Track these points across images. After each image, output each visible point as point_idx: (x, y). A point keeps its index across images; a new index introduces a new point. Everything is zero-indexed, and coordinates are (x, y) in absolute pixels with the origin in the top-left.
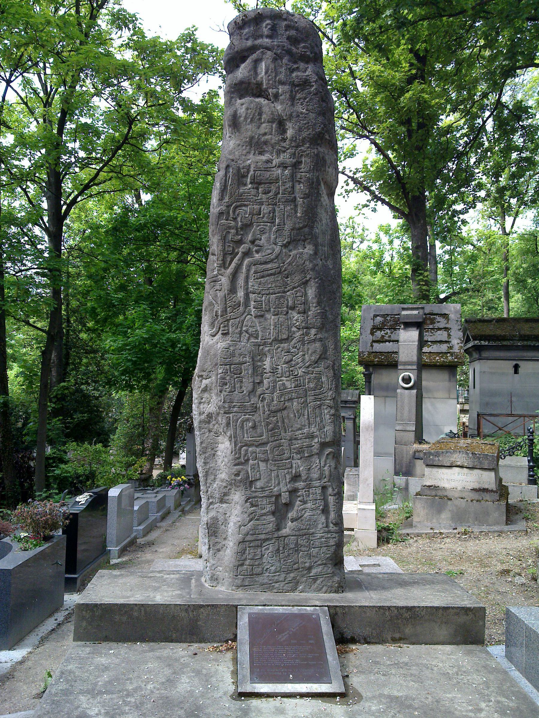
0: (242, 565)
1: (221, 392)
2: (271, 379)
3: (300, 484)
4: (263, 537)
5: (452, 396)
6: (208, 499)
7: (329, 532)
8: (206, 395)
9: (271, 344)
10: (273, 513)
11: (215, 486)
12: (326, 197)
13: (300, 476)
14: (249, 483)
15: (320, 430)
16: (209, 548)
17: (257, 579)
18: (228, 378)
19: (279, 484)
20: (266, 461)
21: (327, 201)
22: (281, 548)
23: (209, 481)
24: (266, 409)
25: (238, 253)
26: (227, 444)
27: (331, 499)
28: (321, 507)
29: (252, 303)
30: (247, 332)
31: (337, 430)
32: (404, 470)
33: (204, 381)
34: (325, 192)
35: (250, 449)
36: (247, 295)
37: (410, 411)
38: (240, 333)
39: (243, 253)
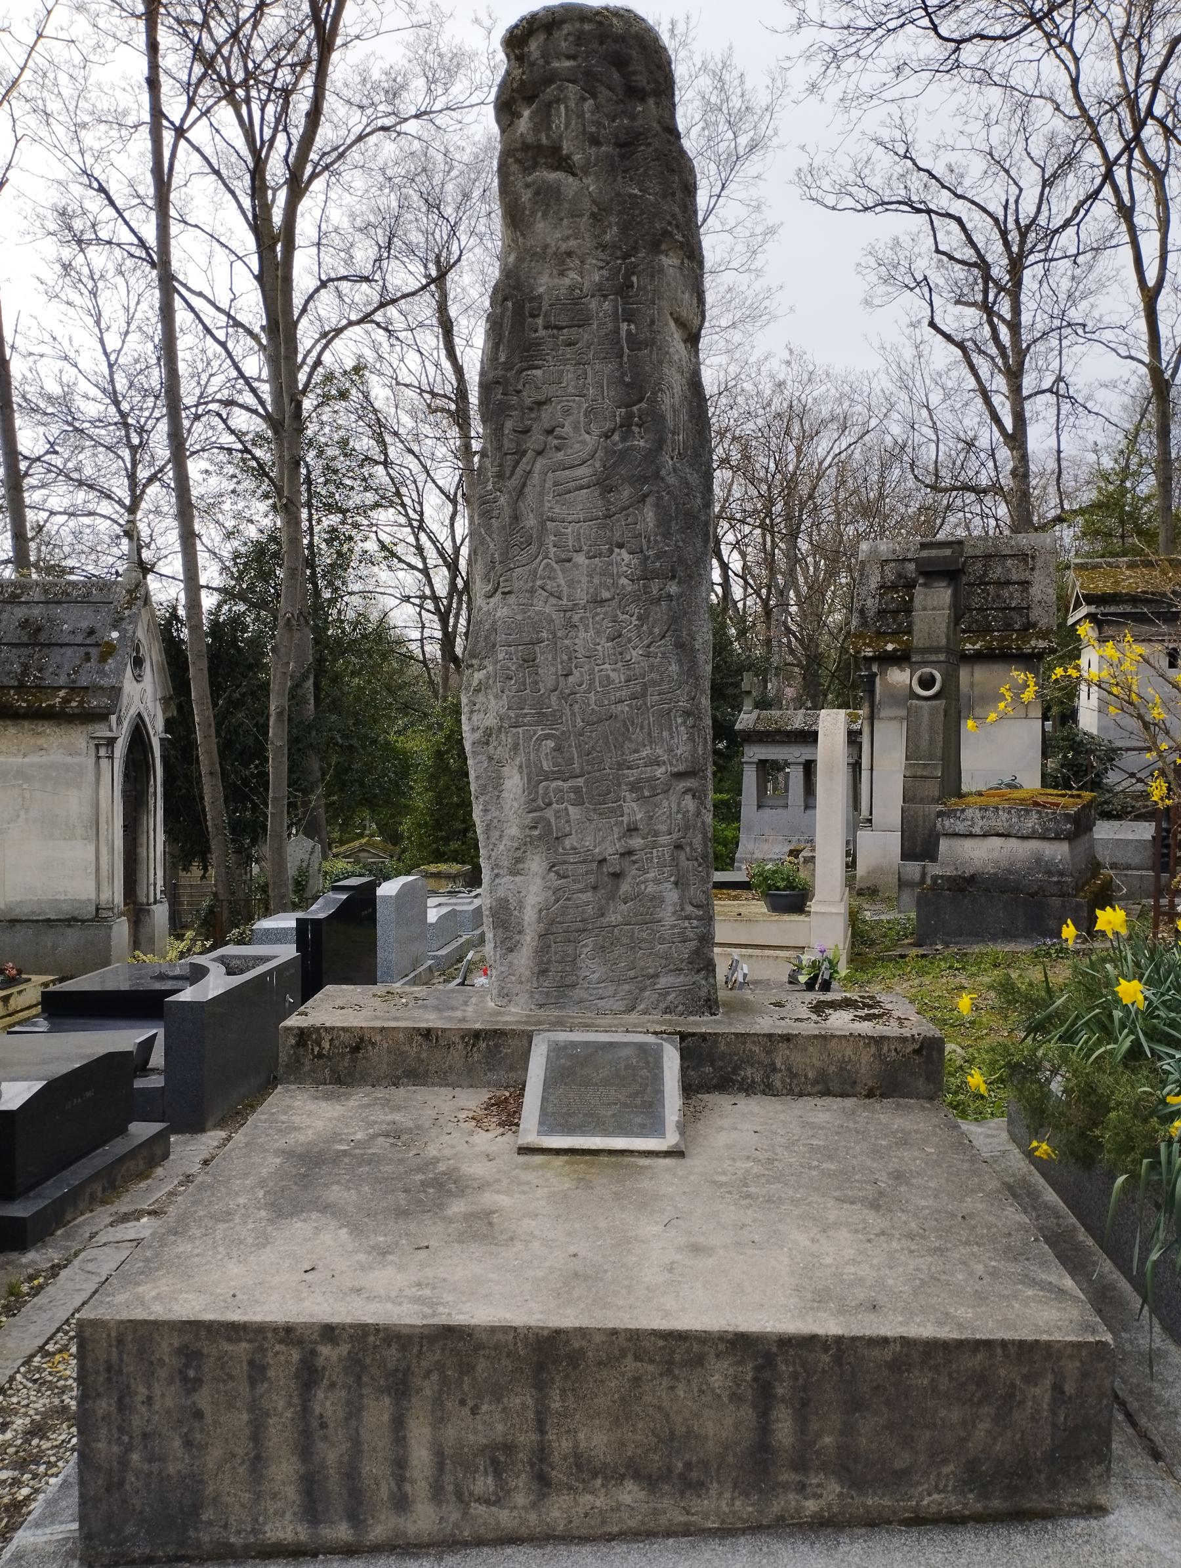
3: (636, 842)
7: (688, 918)
8: (481, 698)
9: (584, 608)
10: (595, 888)
11: (502, 847)
12: (681, 346)
13: (636, 829)
21: (684, 352)
25: (525, 452)
26: (517, 777)
33: (476, 675)
37: (932, 741)
38: (532, 591)
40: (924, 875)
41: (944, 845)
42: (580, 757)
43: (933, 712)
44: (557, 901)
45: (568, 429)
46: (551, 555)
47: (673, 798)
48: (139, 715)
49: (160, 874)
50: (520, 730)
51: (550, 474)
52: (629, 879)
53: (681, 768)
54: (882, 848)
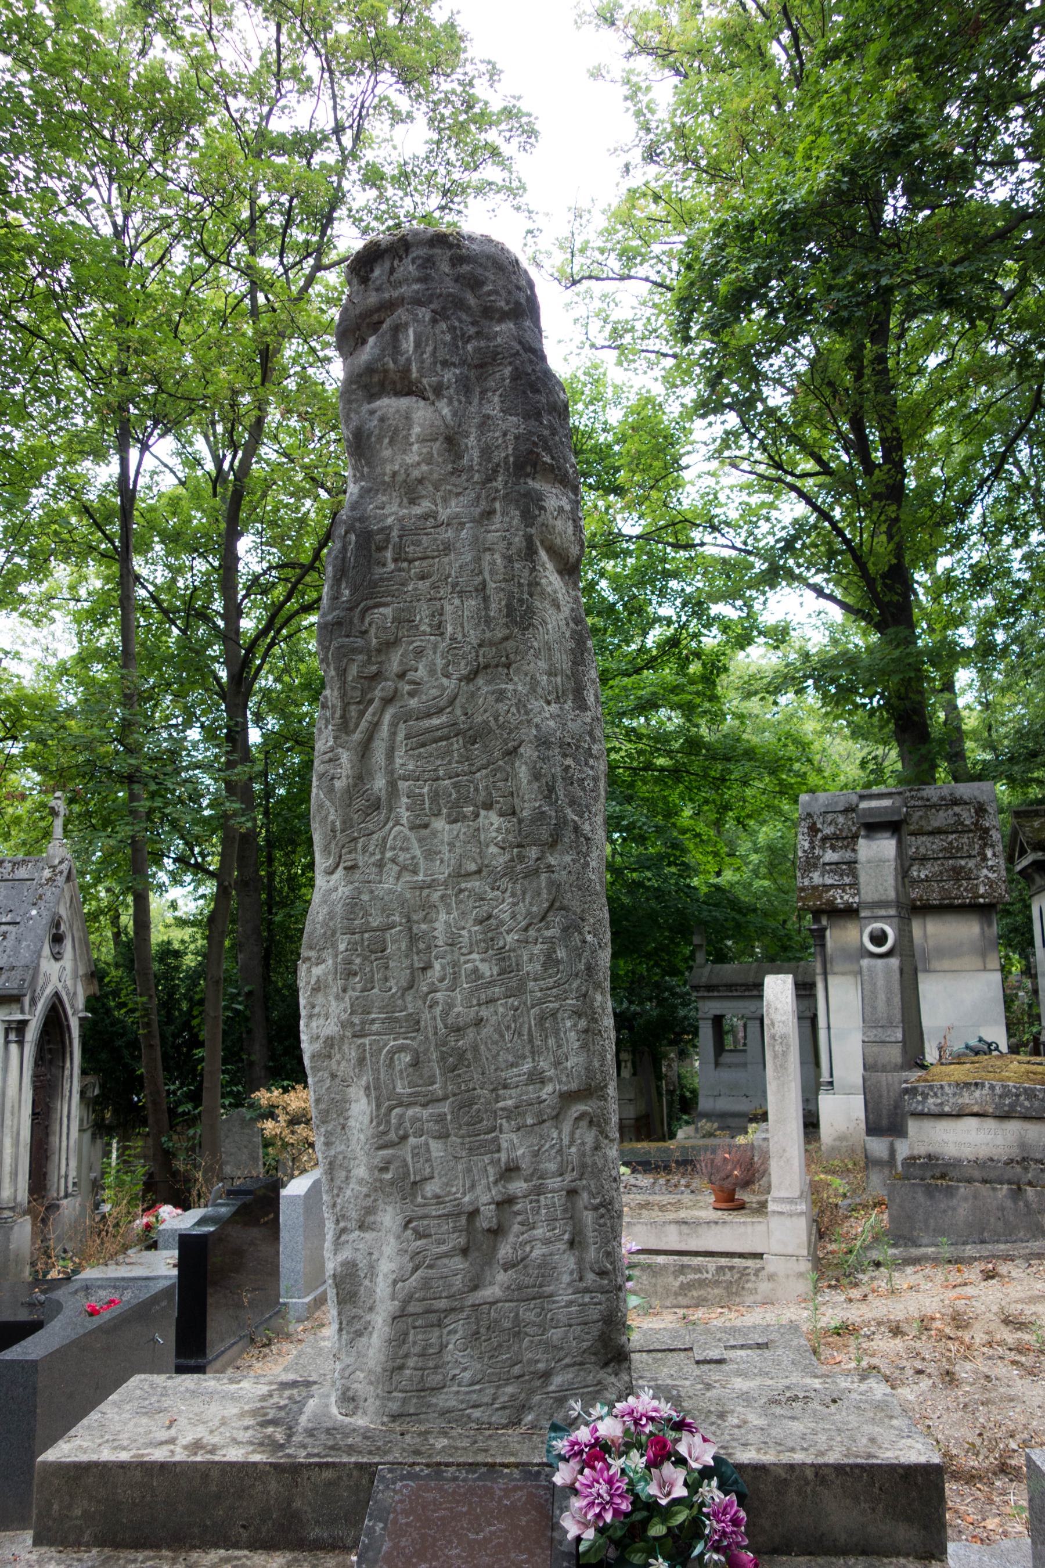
0: (401, 1367)
1: (344, 990)
2: (449, 957)
3: (518, 1186)
4: (443, 1304)
5: (989, 966)
6: (338, 1222)
7: (587, 1290)
8: (320, 999)
9: (445, 884)
10: (465, 1252)
11: (349, 1193)
13: (518, 1169)
14: (408, 1187)
15: (557, 1064)
16: (340, 1330)
17: (434, 1400)
18: (358, 961)
19: (473, 1186)
20: (443, 1136)
22: (483, 1330)
23: (338, 1182)
24: (440, 1025)
25: (371, 701)
26: (364, 1100)
27: (588, 1217)
28: (566, 1237)
29: (404, 800)
30: (393, 861)
31: (597, 1064)
32: (885, 1122)
34: (549, 566)
35: (410, 1112)
36: (392, 784)
37: (889, 1001)
38: (380, 865)
39: (382, 699)
40: (892, 1152)
41: (913, 1126)
42: (443, 1075)
43: (888, 971)
44: (416, 1269)
45: (422, 672)
46: (404, 821)
47: (567, 1127)
48: (57, 994)
49: (73, 1164)
50: (367, 1041)
51: (402, 726)
52: (511, 1239)
53: (574, 1086)
54: (842, 1112)
